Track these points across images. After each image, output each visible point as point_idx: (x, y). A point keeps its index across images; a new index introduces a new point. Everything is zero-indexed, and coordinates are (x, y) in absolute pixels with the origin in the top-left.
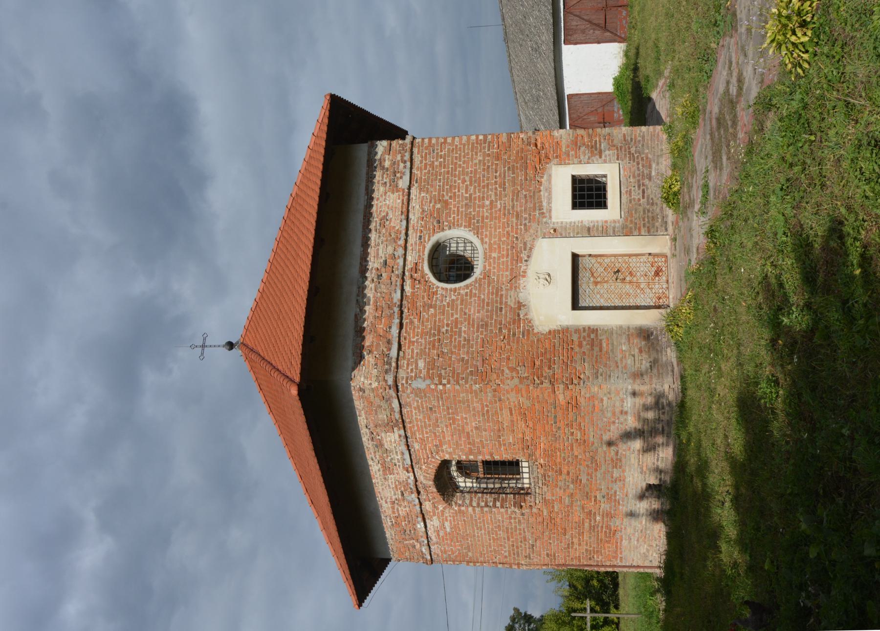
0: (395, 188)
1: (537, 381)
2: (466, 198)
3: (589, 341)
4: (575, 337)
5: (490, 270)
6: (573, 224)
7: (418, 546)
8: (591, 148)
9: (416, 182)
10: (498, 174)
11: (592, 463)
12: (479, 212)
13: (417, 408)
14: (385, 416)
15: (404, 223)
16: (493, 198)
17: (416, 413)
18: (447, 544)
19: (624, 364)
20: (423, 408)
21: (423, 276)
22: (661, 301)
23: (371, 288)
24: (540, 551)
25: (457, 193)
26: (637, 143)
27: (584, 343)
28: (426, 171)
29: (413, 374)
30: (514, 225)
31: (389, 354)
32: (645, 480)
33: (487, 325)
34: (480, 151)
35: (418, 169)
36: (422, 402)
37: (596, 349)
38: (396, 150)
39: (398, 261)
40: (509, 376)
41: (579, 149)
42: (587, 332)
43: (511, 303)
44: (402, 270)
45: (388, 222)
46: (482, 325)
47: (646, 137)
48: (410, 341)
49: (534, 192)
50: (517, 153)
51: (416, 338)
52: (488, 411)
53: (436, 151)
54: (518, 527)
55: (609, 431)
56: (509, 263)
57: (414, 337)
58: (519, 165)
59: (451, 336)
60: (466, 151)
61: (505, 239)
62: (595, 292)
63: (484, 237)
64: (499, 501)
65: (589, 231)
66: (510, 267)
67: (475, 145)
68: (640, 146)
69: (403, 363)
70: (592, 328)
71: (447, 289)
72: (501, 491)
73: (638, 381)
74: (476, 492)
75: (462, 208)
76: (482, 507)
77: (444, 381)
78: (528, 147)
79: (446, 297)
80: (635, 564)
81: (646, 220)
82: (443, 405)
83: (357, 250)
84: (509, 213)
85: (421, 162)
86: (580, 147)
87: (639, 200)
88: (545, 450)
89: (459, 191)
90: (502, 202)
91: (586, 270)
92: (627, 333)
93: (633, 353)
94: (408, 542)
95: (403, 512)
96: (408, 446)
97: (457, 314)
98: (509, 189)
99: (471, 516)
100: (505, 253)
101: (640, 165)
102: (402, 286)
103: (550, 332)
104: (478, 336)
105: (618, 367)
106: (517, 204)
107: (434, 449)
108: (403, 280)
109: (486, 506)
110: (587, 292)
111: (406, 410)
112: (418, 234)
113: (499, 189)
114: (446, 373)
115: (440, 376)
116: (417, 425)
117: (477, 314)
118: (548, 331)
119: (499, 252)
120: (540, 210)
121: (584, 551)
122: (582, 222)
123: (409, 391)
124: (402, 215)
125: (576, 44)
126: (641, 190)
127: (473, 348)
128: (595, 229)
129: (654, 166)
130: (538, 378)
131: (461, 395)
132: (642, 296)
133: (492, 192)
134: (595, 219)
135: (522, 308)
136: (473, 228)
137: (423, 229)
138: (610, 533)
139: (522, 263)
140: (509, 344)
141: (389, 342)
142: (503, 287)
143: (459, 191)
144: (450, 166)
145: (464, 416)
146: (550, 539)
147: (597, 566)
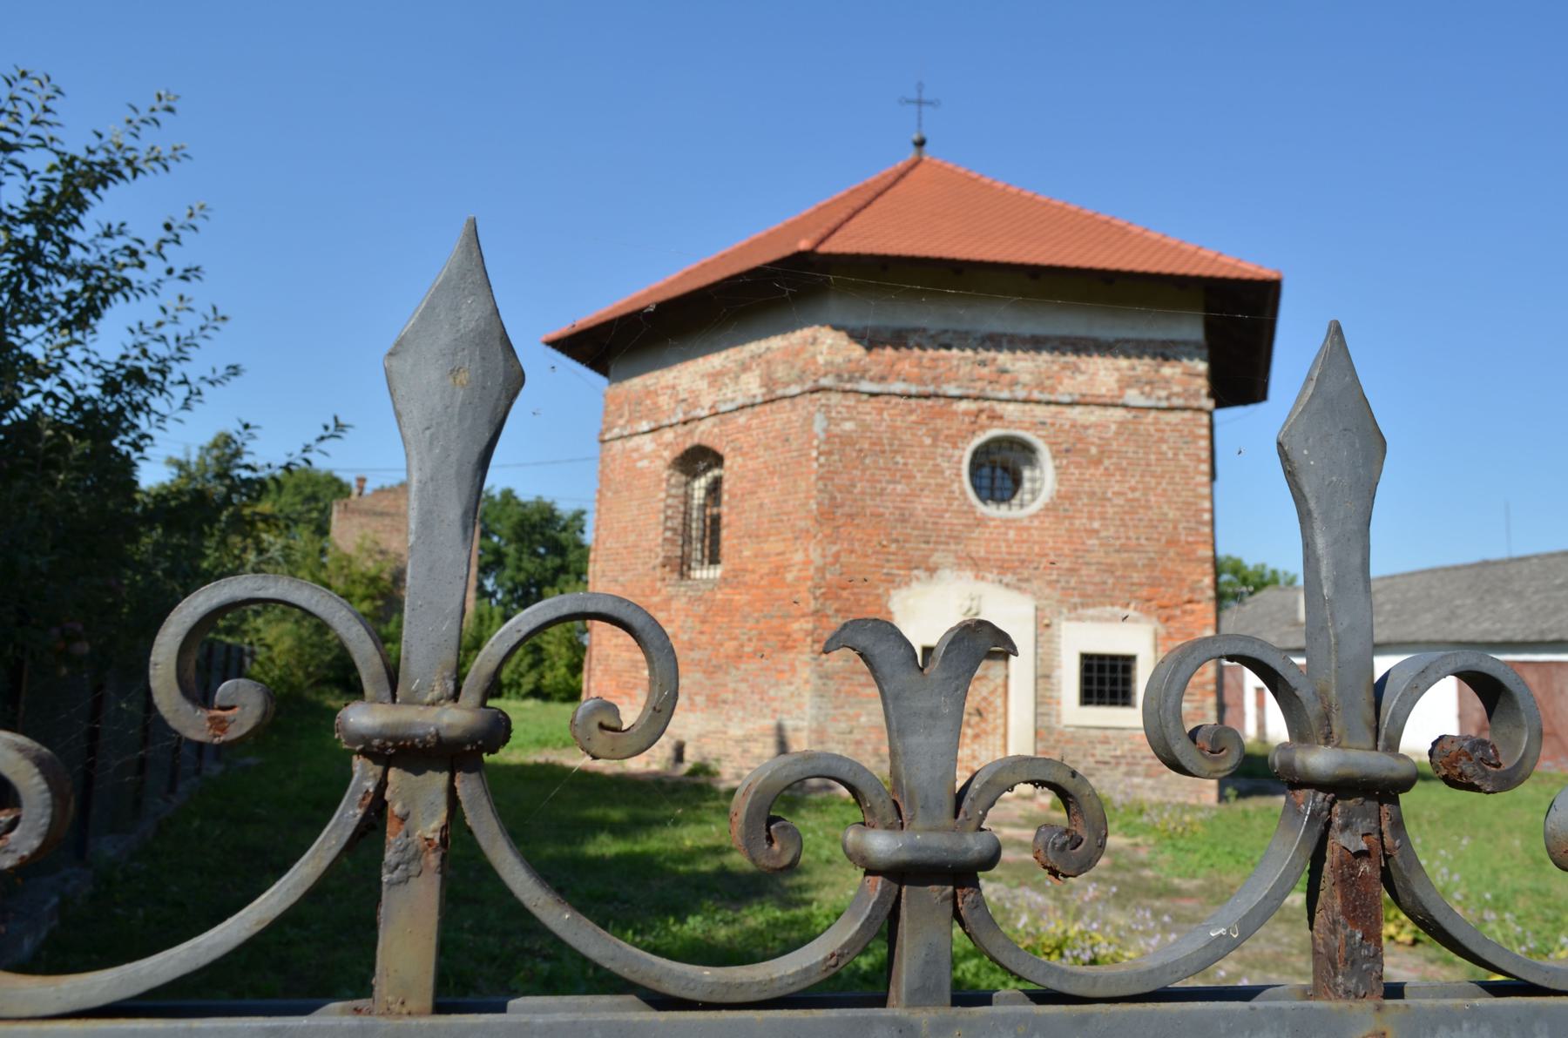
0: (1125, 384)
1: (818, 592)
2: (1104, 493)
7: (621, 422)
11: (714, 666)
12: (1081, 511)
13: (789, 421)
15: (1067, 399)
16: (1104, 534)
21: (983, 428)
33: (904, 521)
35: (1156, 421)
43: (936, 558)
46: (903, 515)
50: (1179, 573)
52: (781, 521)
55: (753, 692)
59: (889, 469)
65: (1044, 676)
69: (851, 400)
72: (687, 540)
77: (822, 459)
83: (1028, 327)
85: (1168, 424)
87: (1093, 755)
88: (732, 600)
95: (664, 401)
104: (887, 508)
107: (738, 444)
108: (976, 398)
109: (667, 518)
115: (830, 453)
129: (1150, 782)
130: (823, 594)
140: (875, 552)
141: (882, 379)
147: (590, 670)
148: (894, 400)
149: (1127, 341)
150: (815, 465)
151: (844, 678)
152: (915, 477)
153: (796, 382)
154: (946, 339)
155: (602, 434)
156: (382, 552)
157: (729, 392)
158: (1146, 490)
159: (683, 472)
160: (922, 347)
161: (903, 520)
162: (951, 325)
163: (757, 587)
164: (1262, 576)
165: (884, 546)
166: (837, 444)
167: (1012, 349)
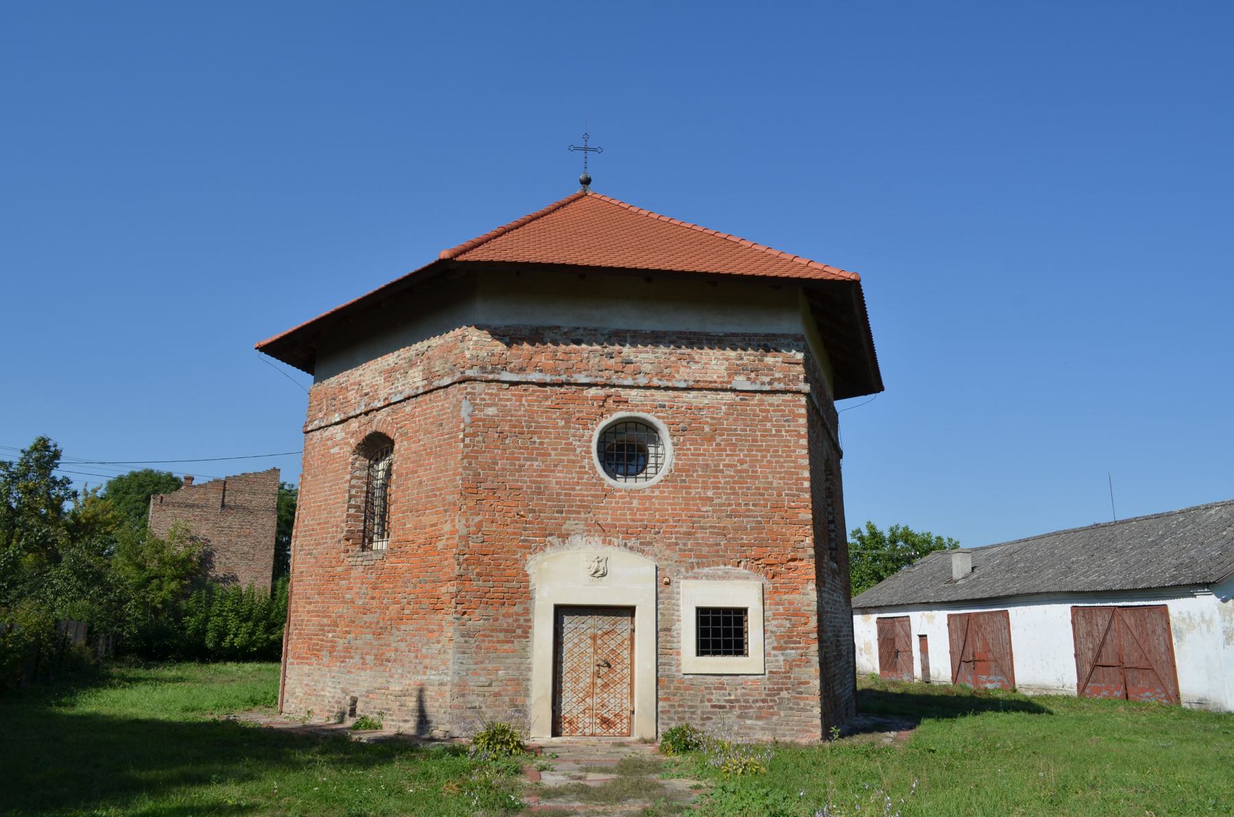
0: (734, 371)
1: (462, 558)
3: (513, 626)
6: (676, 608)
7: (321, 415)
8: (788, 636)
14: (437, 369)
15: (683, 385)
17: (438, 406)
18: (320, 450)
19: (480, 672)
21: (610, 411)
22: (567, 725)
24: (305, 563)
25: (724, 453)
27: (510, 620)
28: (758, 412)
29: (478, 401)
32: (361, 696)
33: (539, 494)
34: (785, 484)
35: (761, 403)
36: (448, 413)
37: (501, 636)
38: (789, 371)
39: (630, 379)
41: (786, 619)
42: (525, 624)
43: (569, 525)
44: (616, 384)
46: (540, 488)
47: (803, 714)
48: (521, 396)
49: (724, 556)
51: (526, 404)
52: (435, 496)
53: (786, 424)
56: (623, 522)
57: (527, 401)
58: (763, 535)
59: (527, 448)
60: (785, 464)
61: (657, 517)
62: (583, 637)
65: (664, 631)
66: (618, 523)
67: (795, 477)
68: (791, 705)
69: (494, 388)
70: (530, 630)
71: (590, 441)
75: (703, 460)
76: (349, 491)
78: (790, 549)
79: (579, 441)
80: (287, 680)
81: (680, 710)
82: (445, 440)
83: (649, 324)
85: (771, 405)
86: (790, 620)
89: (727, 455)
90: (710, 514)
91: (613, 625)
92: (521, 678)
93: (494, 684)
95: (352, 395)
96: (409, 398)
97: (556, 455)
98: (727, 523)
100: (638, 517)
102: (596, 385)
103: (527, 575)
105: (476, 664)
108: (604, 386)
110: (582, 626)
112: (667, 404)
113: (730, 508)
114: (478, 442)
115: (475, 435)
116: (427, 409)
117: (554, 480)
118: (528, 572)
119: (638, 509)
120: (698, 563)
122: (679, 620)
123: (459, 396)
124: (694, 381)
125: (1073, 623)
126: (724, 704)
127: (510, 476)
128: (669, 638)
129: (760, 723)
130: (466, 560)
131: (452, 462)
132: (574, 700)
134: (682, 638)
135: (560, 539)
136: (673, 475)
137: (675, 409)
138: (317, 650)
139: (623, 539)
141: (522, 370)
142: (591, 514)
143: (727, 455)
144: (764, 444)
146: (316, 575)
148: (532, 388)
149: (733, 335)
150: (462, 445)
151: (485, 636)
152: (550, 455)
153: (448, 375)
154: (574, 336)
155: (306, 426)
156: (192, 539)
157: (399, 385)
158: (753, 462)
159: (366, 456)
160: (556, 343)
161: (540, 493)
162: (582, 324)
163: (415, 555)
164: (929, 543)
166: (479, 426)
167: (633, 344)
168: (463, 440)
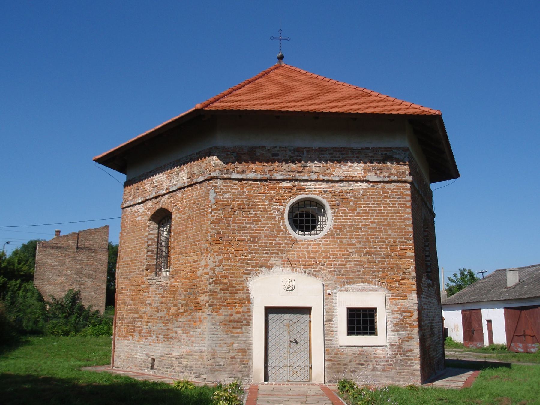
1: (211, 280)
4: (244, 309)
5: (298, 244)
7: (131, 198)
9: (372, 186)
10: (378, 249)
14: (195, 172)
15: (337, 179)
16: (358, 246)
20: (199, 198)
21: (295, 195)
23: (285, 157)
26: (404, 361)
30: (335, 263)
31: (235, 172)
32: (157, 358)
36: (202, 197)
38: (400, 169)
39: (306, 176)
40: (216, 260)
41: (400, 314)
45: (339, 167)
46: (255, 240)
48: (244, 187)
50: (397, 264)
52: (196, 245)
53: (399, 200)
54: (137, 267)
58: (386, 265)
60: (398, 224)
63: (325, 239)
64: (152, 254)
65: (328, 320)
68: (403, 363)
69: (228, 183)
73: (210, 355)
74: (158, 237)
78: (402, 273)
80: (116, 349)
83: (317, 144)
84: (345, 258)
85: (389, 189)
89: (364, 219)
94: (133, 191)
97: (264, 221)
98: (364, 259)
99: (143, 235)
100: (312, 256)
101: (385, 363)
104: (247, 236)
106: (352, 265)
108: (291, 180)
109: (148, 246)
111: (198, 186)
114: (220, 214)
115: (217, 210)
119: (312, 251)
121: (123, 314)
124: (344, 176)
131: (205, 225)
133: (363, 245)
139: (304, 268)
143: (364, 219)
145: (194, 228)
147: (116, 323)
155: (123, 205)
165: (245, 256)
168: (211, 213)
